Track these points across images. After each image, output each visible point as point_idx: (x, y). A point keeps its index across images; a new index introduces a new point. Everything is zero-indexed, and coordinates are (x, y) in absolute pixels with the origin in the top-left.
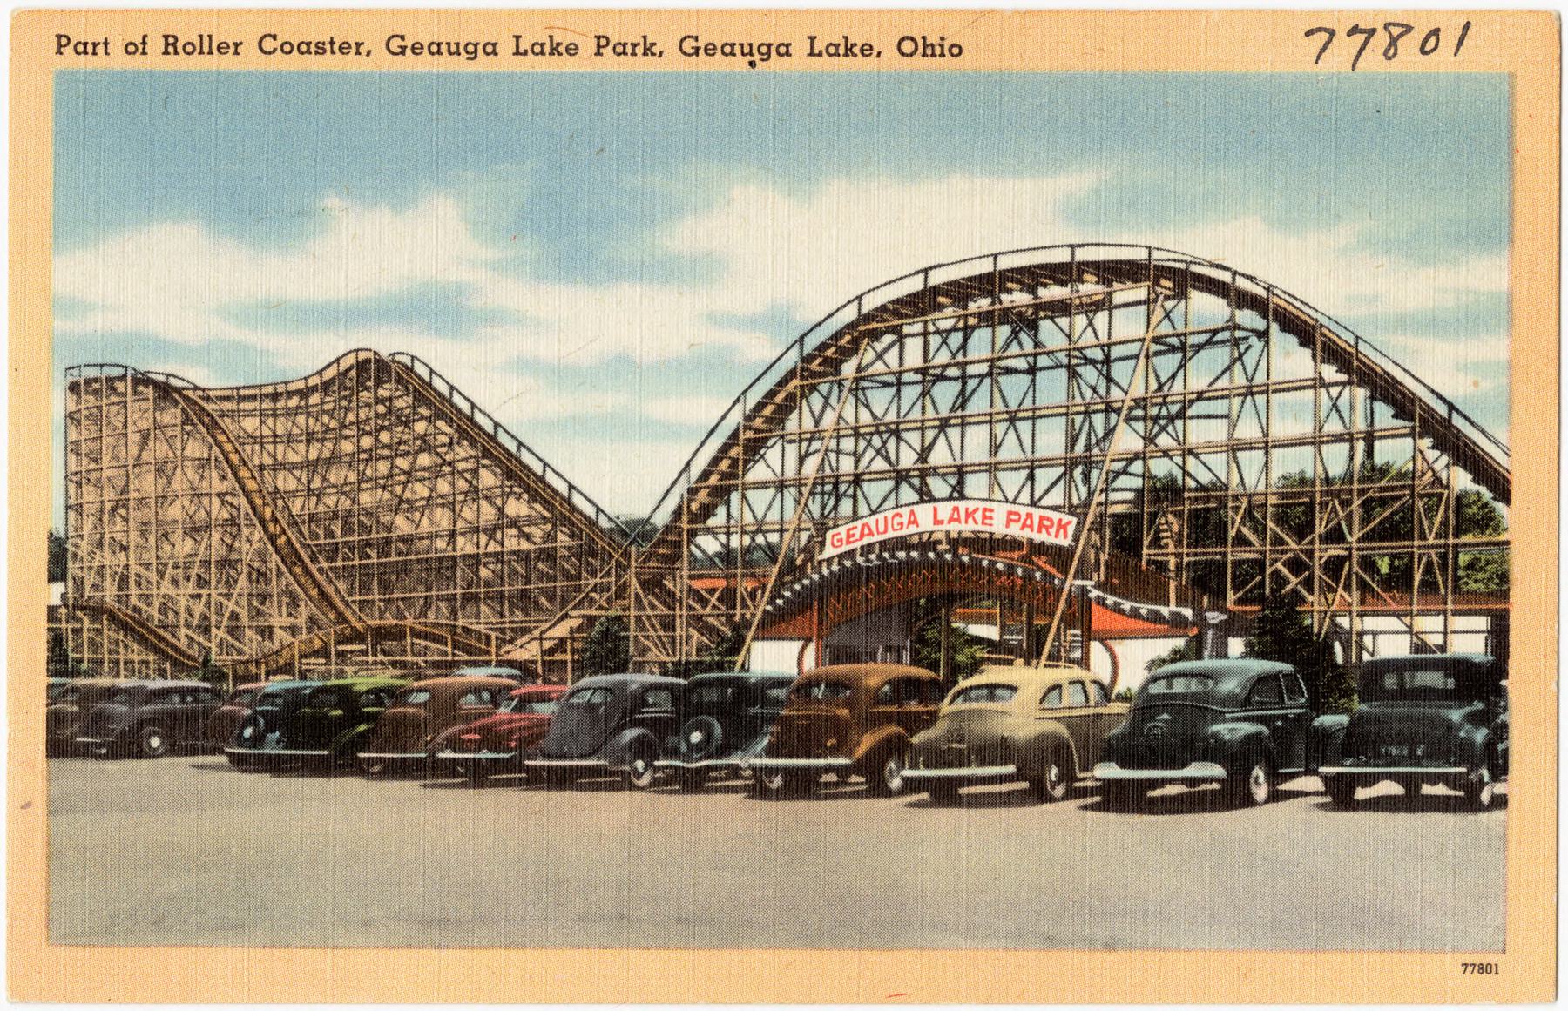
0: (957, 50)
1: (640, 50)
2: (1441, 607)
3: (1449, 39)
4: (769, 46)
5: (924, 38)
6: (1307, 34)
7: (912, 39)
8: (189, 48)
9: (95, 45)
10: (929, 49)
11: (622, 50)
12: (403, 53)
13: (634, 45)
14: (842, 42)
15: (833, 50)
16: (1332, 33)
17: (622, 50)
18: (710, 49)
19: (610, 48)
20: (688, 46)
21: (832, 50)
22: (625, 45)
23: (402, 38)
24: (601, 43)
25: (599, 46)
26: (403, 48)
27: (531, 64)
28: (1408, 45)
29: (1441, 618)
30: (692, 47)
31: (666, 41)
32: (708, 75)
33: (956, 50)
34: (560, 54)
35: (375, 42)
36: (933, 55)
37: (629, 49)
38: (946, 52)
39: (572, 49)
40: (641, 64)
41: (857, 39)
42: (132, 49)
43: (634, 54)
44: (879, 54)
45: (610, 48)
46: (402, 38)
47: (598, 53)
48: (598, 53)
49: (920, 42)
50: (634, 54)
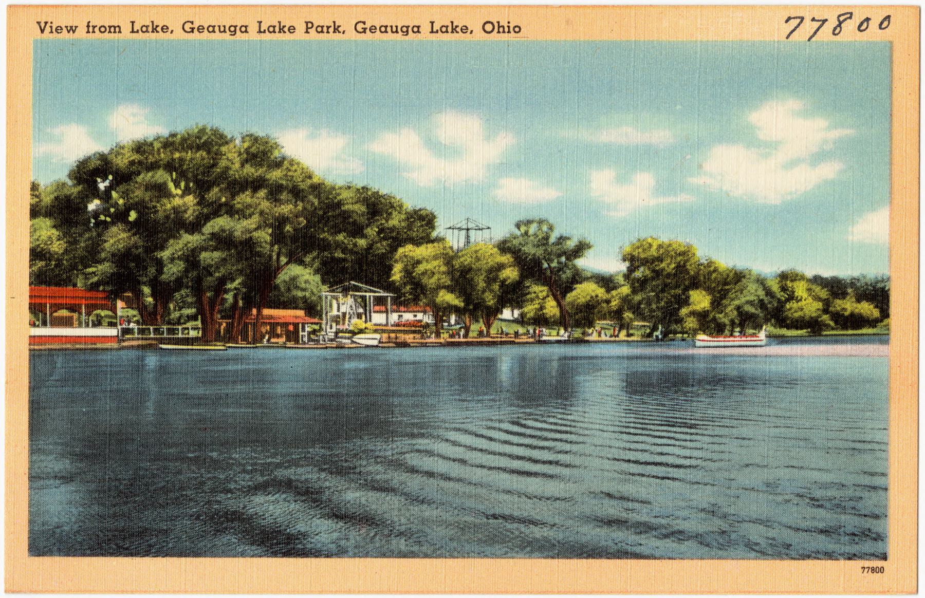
0: (518, 29)
1: (331, 30)
2: (383, 308)
3: (874, 24)
4: (235, 27)
5: (498, 22)
6: (787, 21)
7: (492, 23)
8: (103, 29)
9: (328, 27)
10: (500, 29)
11: (321, 30)
12: (192, 32)
13: (328, 27)
14: (278, 25)
15: (444, 30)
16: (802, 19)
17: (321, 30)
18: (373, 29)
19: (314, 28)
20: (360, 27)
21: (144, 29)
22: (322, 27)
23: (364, 23)
24: (309, 26)
25: (307, 28)
26: (193, 29)
27: (267, 36)
28: (850, 27)
29: (385, 315)
30: (362, 28)
31: (347, 25)
32: (145, 43)
33: (517, 29)
34: (285, 32)
35: (176, 26)
36: (504, 32)
37: (325, 29)
38: (54, 30)
39: (292, 29)
40: (332, 36)
41: (459, 23)
42: (517, 29)
43: (328, 32)
44: (172, 32)
45: (314, 28)
46: (192, 23)
47: (307, 32)
48: (307, 32)
49: (496, 25)
50: (328, 32)
